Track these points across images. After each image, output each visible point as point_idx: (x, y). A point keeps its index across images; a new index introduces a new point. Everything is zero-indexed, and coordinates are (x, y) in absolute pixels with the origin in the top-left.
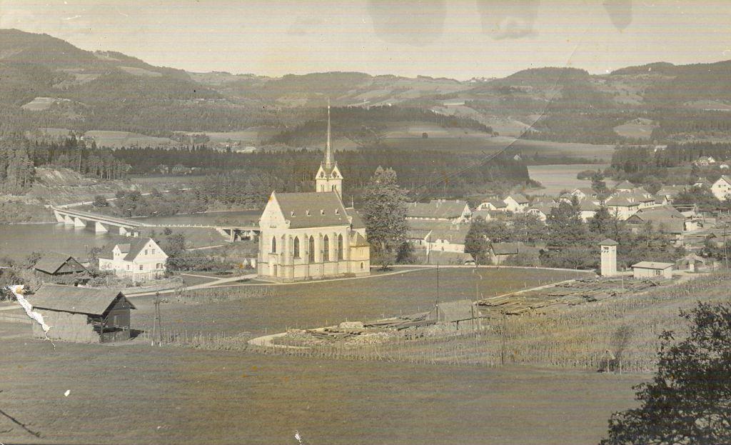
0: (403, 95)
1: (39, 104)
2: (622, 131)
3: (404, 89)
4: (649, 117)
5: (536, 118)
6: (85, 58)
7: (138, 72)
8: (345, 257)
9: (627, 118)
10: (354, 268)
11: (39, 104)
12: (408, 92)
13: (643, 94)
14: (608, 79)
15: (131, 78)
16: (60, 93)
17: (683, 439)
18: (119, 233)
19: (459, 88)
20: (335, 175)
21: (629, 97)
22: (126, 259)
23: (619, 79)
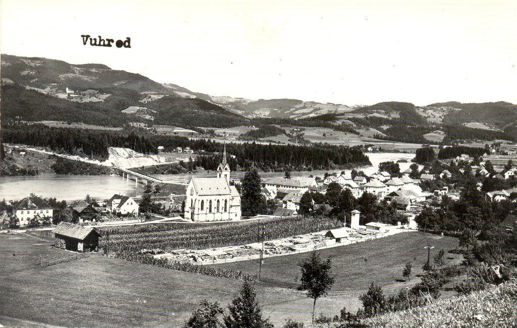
0: (319, 112)
1: (131, 110)
2: (428, 136)
3: (319, 109)
4: (443, 130)
5: (385, 127)
6: (157, 87)
7: (184, 95)
8: (228, 210)
9: (432, 130)
10: (232, 216)
11: (131, 110)
12: (321, 110)
13: (443, 118)
14: (425, 109)
15: (179, 98)
16: (142, 105)
17: (375, 308)
18: (54, 211)
19: (348, 110)
20: (226, 169)
21: (436, 117)
22: (374, 135)
23: (431, 109)
